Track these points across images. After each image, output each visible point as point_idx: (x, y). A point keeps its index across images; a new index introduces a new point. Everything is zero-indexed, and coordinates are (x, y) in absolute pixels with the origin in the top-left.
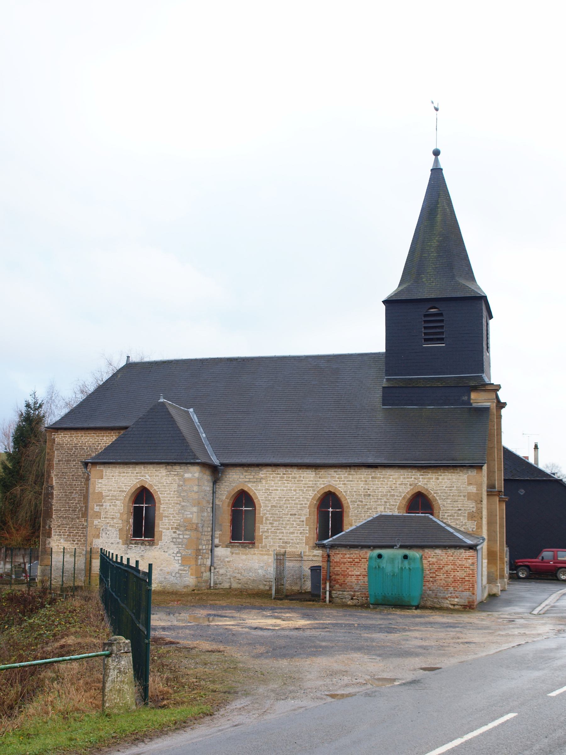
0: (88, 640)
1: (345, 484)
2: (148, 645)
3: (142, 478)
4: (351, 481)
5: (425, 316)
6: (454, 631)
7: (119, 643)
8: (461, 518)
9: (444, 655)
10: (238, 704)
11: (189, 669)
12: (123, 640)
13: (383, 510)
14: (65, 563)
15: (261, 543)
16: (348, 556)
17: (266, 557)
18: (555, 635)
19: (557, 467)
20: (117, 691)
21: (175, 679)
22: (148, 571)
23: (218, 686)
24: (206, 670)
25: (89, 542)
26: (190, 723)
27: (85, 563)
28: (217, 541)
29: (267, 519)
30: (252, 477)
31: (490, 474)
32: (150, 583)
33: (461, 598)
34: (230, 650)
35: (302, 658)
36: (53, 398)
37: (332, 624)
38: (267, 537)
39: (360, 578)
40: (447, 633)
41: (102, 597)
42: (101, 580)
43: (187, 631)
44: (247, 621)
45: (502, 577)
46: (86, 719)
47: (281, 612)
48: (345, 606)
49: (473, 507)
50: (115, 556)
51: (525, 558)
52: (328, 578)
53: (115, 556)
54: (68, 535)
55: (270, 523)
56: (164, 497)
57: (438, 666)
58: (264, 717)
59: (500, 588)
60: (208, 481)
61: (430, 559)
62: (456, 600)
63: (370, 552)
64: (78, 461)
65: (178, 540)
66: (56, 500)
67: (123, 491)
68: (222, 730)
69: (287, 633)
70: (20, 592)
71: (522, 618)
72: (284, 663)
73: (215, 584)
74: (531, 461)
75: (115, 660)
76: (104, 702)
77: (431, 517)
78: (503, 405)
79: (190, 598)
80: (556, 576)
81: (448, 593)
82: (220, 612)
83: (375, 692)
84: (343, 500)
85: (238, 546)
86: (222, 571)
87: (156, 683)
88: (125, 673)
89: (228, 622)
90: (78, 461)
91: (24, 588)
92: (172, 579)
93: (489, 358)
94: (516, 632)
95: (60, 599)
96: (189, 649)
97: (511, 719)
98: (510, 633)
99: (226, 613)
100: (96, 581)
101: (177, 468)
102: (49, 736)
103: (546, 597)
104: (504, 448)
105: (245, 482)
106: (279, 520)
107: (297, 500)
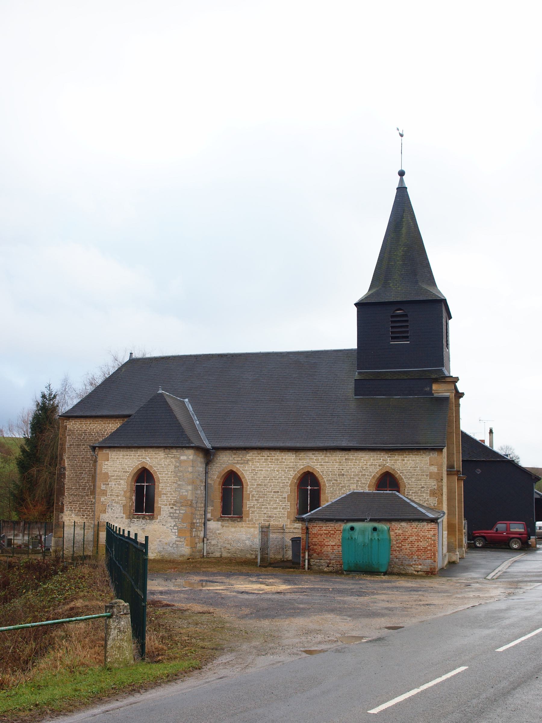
0: (94, 603)
1: (321, 465)
2: (145, 607)
3: (143, 460)
4: (328, 462)
5: (392, 316)
6: (417, 595)
7: (119, 606)
8: (424, 495)
9: (407, 616)
10: (223, 659)
11: (182, 628)
12: (122, 603)
13: (355, 488)
14: (76, 535)
15: (248, 517)
16: (324, 528)
17: (252, 529)
18: (506, 597)
19: (511, 449)
20: (117, 648)
21: (170, 637)
22: (144, 542)
23: (207, 644)
24: (197, 629)
25: (96, 516)
26: (181, 676)
27: (94, 535)
28: (209, 516)
29: (253, 496)
30: (240, 459)
31: (450, 456)
32: (146, 553)
33: (424, 565)
34: (219, 612)
35: (282, 619)
36: (67, 390)
37: (310, 589)
38: (253, 512)
39: (336, 547)
40: (411, 596)
41: (107, 565)
42: (107, 550)
43: (182, 595)
44: (235, 586)
45: (460, 546)
46: (90, 672)
47: (265, 578)
48: (321, 572)
49: (434, 485)
50: (118, 529)
51: (481, 529)
52: (307, 548)
53: (118, 529)
54: (78, 511)
55: (256, 500)
56: (163, 477)
57: (401, 625)
58: (246, 670)
59: (458, 556)
60: (201, 463)
61: (397, 531)
62: (420, 567)
63: (344, 525)
64: (87, 445)
65: (175, 515)
66: (68, 480)
67: (126, 472)
68: (209, 682)
69: (269, 596)
70: (36, 561)
71: (477, 583)
72: (266, 623)
73: (208, 553)
74: (487, 444)
75: (115, 621)
76: (106, 657)
77: (398, 494)
78: (461, 395)
79: (185, 566)
80: (509, 546)
81: (412, 561)
82: (211, 578)
83: (345, 648)
84: (320, 479)
85: (228, 520)
86: (213, 542)
87: (152, 640)
88: (125, 633)
89: (218, 587)
90: (87, 445)
91: (39, 557)
92: (170, 549)
93: (448, 353)
94: (471, 595)
95: (71, 567)
96: (182, 611)
97: (462, 671)
98: (466, 596)
99: (217, 579)
100: (102, 551)
101: (174, 451)
102: (56, 687)
103: (499, 564)
104: (462, 432)
105: (234, 463)
106: (264, 497)
107: (280, 479)
